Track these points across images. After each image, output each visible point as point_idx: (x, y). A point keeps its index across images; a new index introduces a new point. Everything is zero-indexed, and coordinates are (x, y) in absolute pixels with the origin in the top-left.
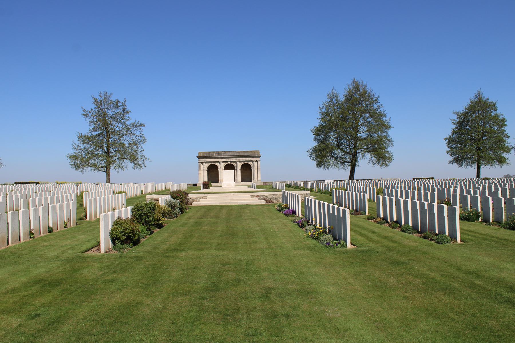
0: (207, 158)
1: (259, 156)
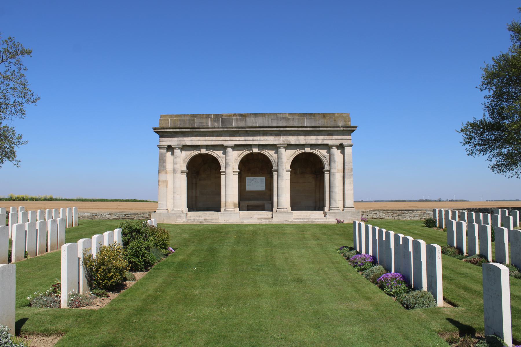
0: (184, 134)
1: (349, 130)
